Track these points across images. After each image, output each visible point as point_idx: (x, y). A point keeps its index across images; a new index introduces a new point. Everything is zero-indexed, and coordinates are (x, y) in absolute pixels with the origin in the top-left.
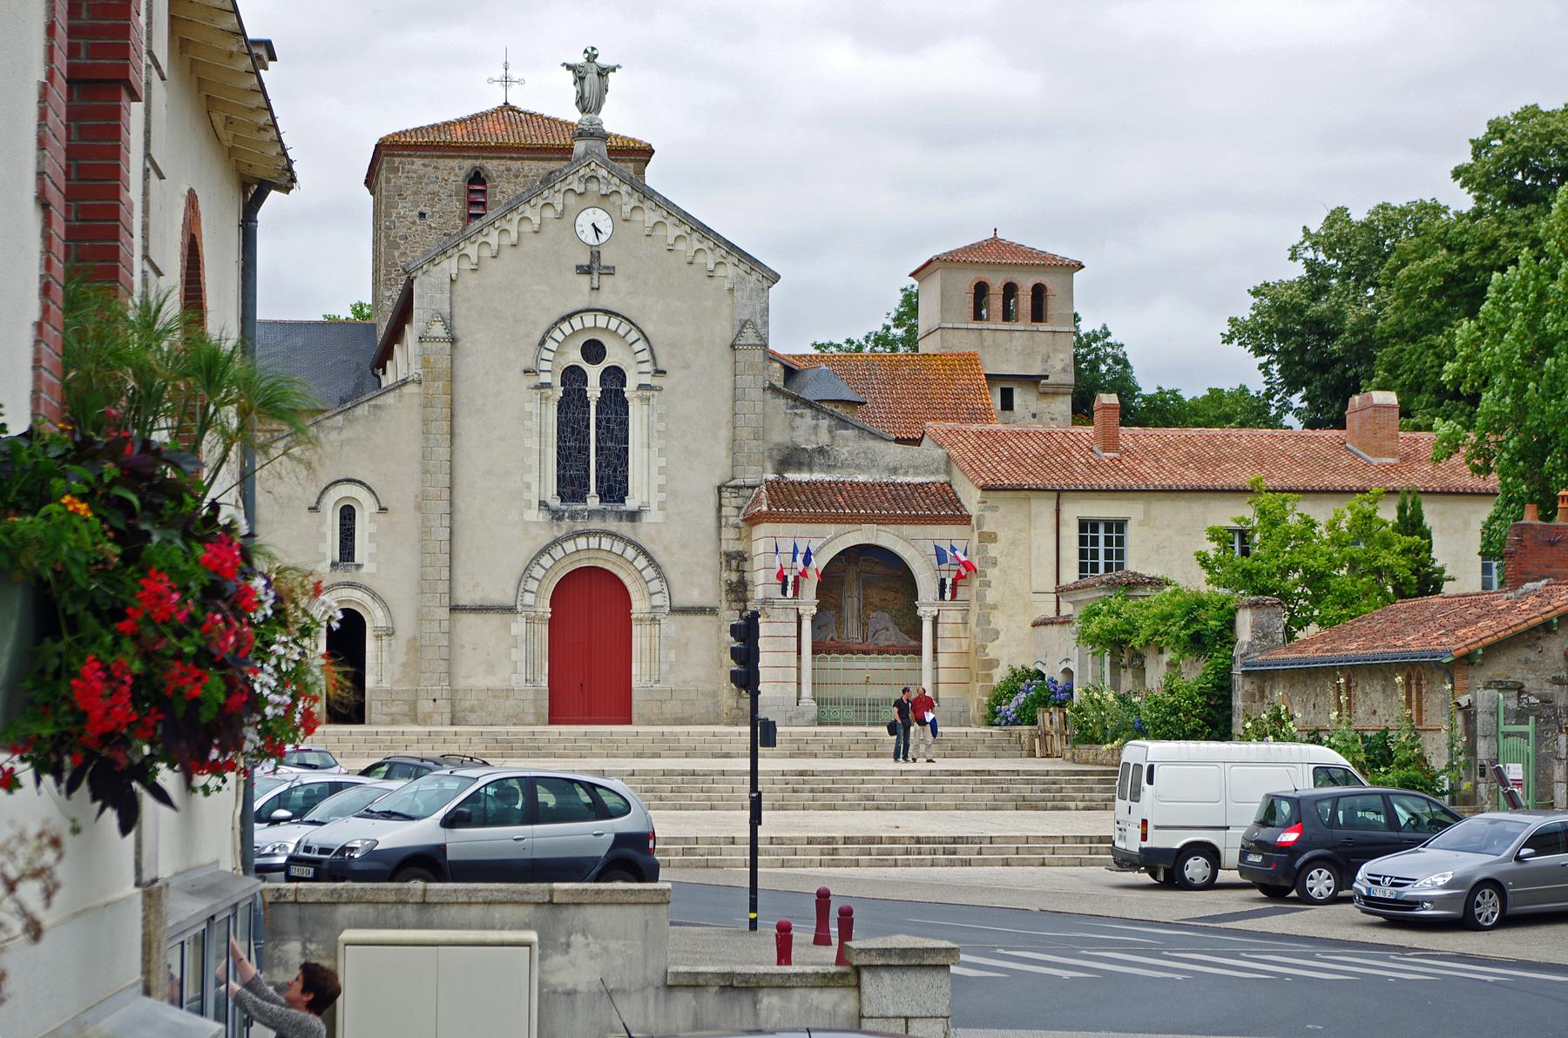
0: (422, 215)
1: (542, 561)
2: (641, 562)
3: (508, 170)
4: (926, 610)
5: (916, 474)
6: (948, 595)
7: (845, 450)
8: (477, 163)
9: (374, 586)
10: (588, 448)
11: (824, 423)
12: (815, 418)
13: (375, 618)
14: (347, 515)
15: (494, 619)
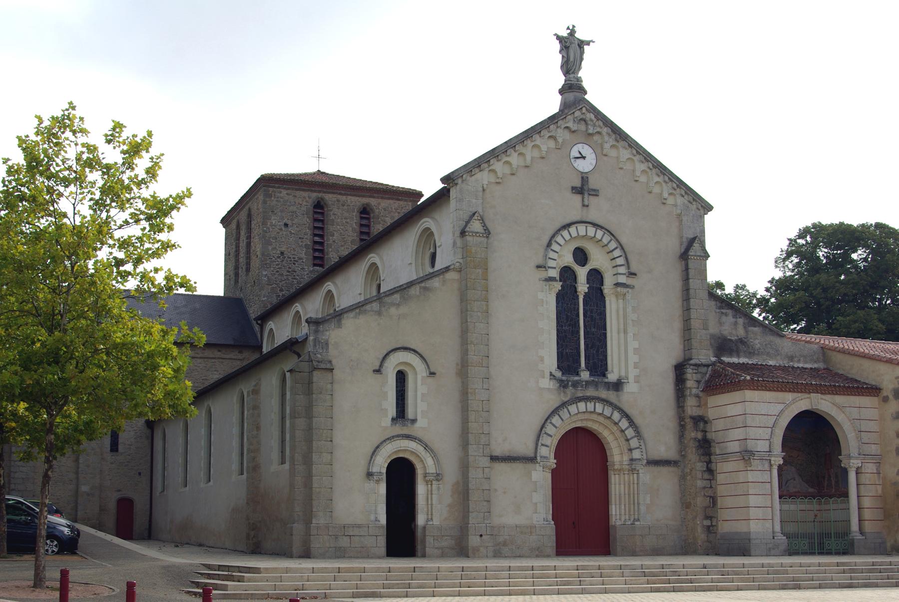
0: (286, 225)
2: (624, 424)
3: (338, 201)
5: (806, 362)
7: (757, 342)
8: (320, 195)
9: (426, 439)
10: (578, 332)
11: (741, 321)
12: (734, 317)
13: (425, 465)
14: (401, 377)
15: (519, 466)
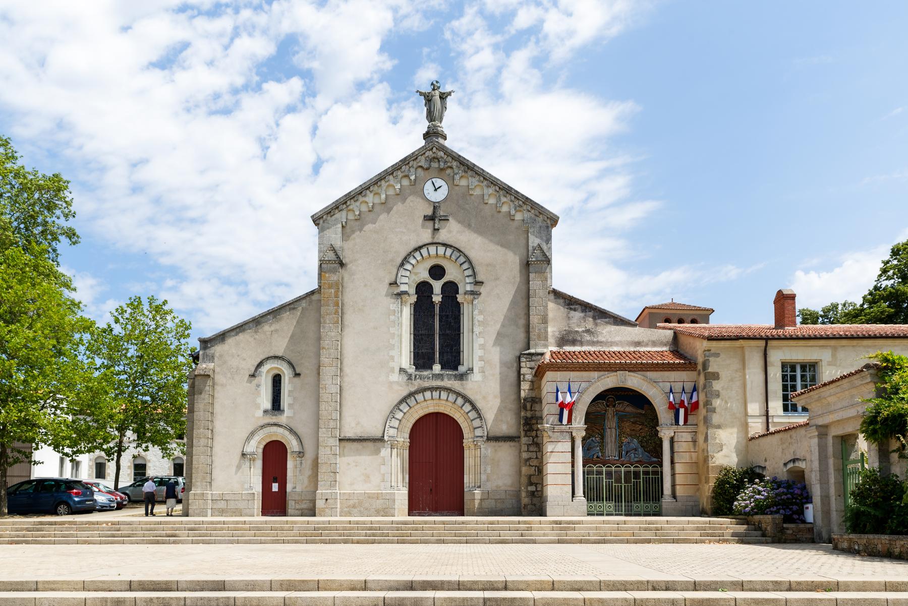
1: (434, 393)
4: (665, 434)
6: (681, 421)
14: (277, 381)
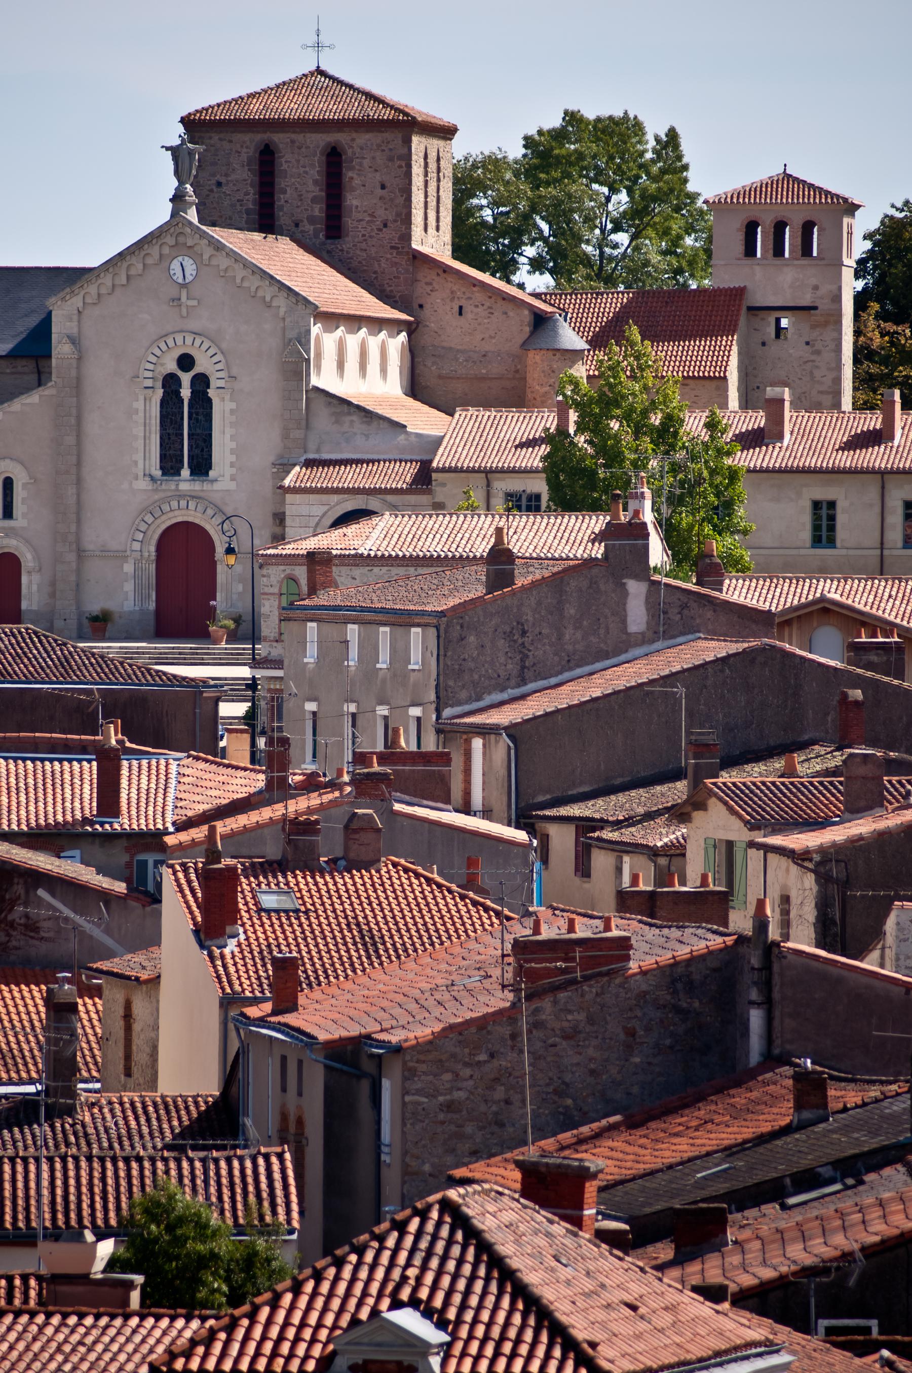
0: (219, 184)
3: (293, 142)
10: (182, 435)
